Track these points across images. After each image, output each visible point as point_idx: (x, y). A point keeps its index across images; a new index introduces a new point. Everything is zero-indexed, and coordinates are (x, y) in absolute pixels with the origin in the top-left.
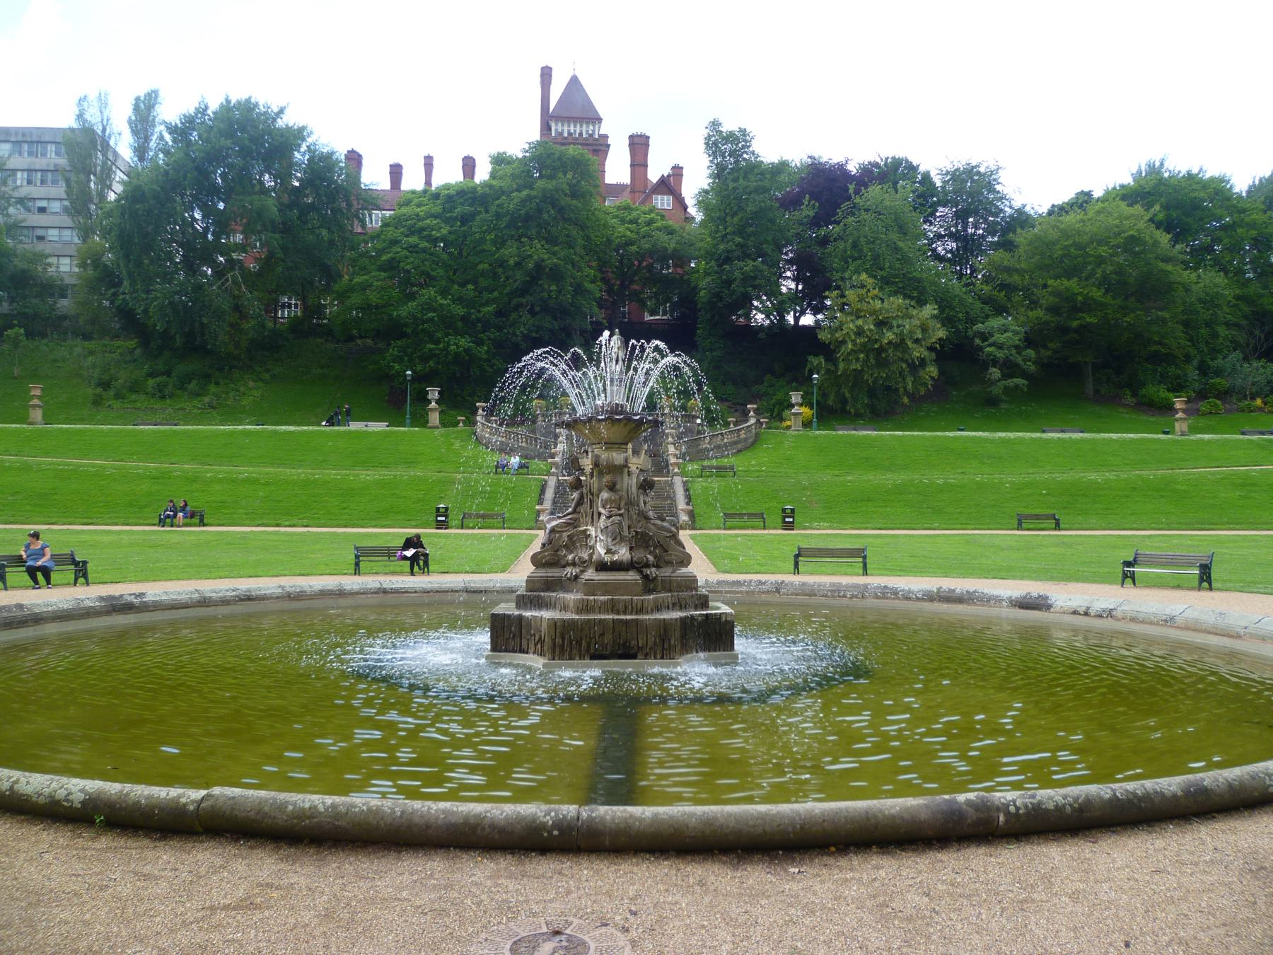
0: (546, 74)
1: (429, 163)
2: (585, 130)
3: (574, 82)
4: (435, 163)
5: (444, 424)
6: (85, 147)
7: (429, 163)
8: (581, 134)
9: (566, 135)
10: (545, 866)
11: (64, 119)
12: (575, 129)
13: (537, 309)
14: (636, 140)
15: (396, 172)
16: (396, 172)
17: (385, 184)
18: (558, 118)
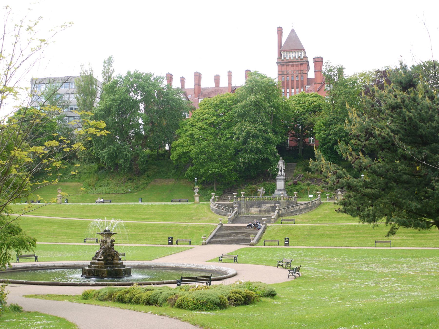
0: (280, 31)
1: (230, 75)
2: (300, 55)
3: (293, 31)
4: (233, 75)
5: (200, 200)
6: (87, 85)
7: (230, 75)
8: (290, 58)
9: (288, 58)
10: (187, 266)
11: (76, 72)
12: (292, 55)
13: (267, 175)
14: (317, 60)
15: (217, 79)
16: (217, 79)
17: (211, 85)
18: (285, 51)
